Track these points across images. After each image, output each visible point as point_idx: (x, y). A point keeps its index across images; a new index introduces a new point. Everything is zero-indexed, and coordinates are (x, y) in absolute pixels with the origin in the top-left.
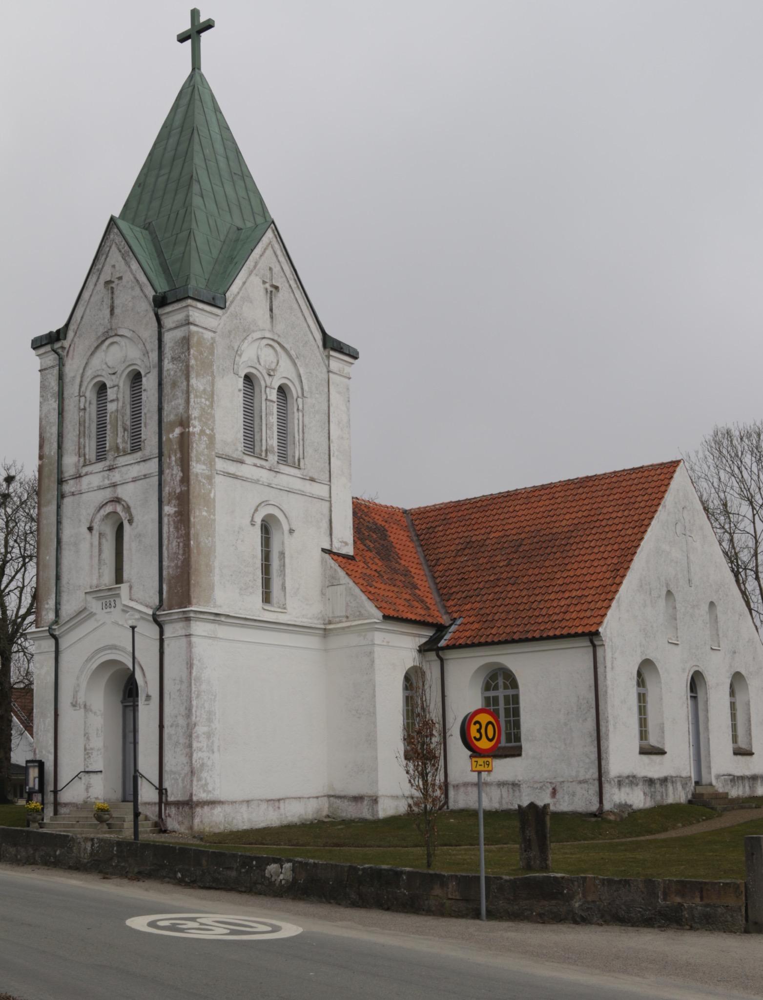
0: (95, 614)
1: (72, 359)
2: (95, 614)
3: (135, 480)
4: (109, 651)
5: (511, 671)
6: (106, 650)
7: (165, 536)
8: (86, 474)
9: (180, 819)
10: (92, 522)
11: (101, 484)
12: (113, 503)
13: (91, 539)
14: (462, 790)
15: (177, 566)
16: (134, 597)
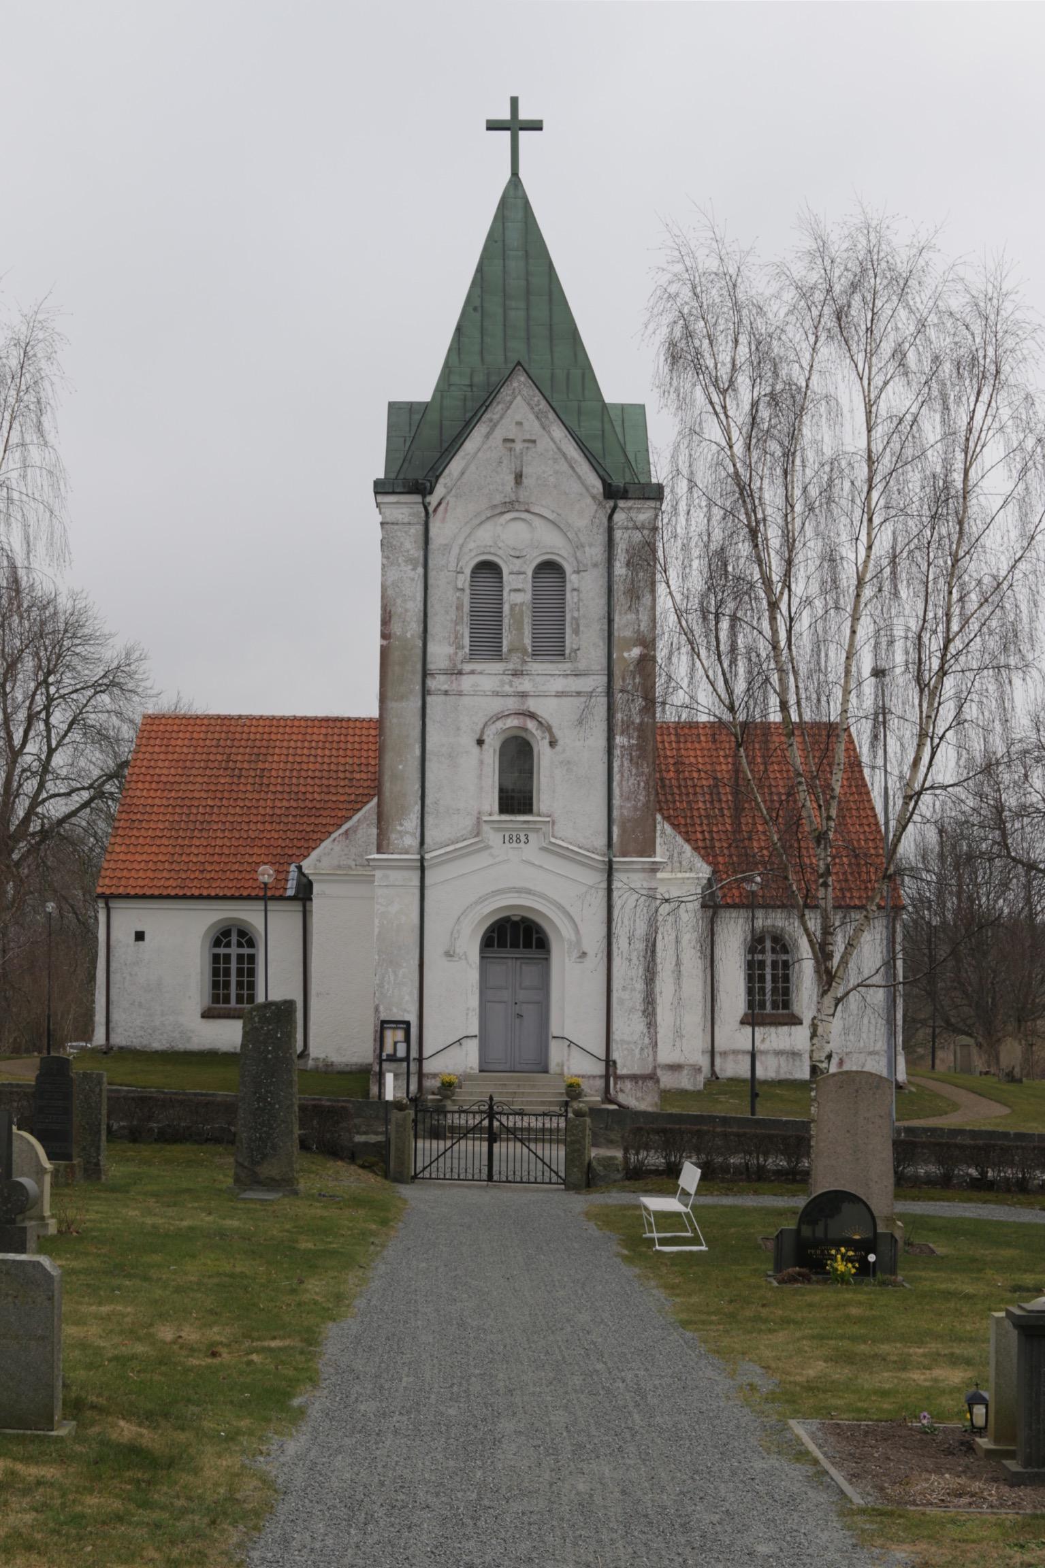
0: (491, 847)
1: (443, 520)
2: (491, 847)
3: (559, 695)
4: (516, 895)
5: (548, 939)
6: (510, 892)
7: (616, 769)
8: (472, 672)
9: (639, 1094)
10: (482, 733)
11: (498, 689)
12: (521, 716)
13: (481, 754)
14: (731, 1057)
15: (635, 808)
16: (556, 834)
